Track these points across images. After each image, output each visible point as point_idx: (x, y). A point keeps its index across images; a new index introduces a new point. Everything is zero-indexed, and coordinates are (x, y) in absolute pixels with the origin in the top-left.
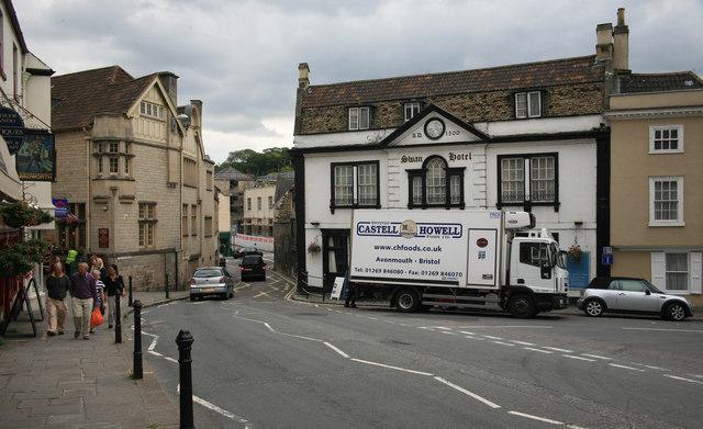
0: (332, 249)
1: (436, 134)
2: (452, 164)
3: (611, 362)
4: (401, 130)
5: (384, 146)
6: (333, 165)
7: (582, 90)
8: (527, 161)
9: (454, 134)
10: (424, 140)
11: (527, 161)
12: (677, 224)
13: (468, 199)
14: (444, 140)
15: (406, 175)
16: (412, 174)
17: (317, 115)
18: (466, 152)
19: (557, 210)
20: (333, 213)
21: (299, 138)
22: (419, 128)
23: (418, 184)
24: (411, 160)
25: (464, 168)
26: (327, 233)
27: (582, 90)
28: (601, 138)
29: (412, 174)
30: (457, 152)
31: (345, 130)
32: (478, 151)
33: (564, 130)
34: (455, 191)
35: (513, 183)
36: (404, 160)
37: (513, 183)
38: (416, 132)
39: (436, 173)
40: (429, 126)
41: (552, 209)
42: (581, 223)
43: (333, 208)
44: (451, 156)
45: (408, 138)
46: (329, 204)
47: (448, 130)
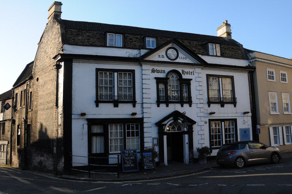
0: (97, 135)
1: (173, 57)
2: (185, 77)
3: (122, 184)
4: (152, 51)
5: (139, 61)
6: (97, 70)
7: (232, 48)
8: (116, 74)
9: (183, 58)
10: (166, 59)
11: (116, 74)
12: (277, 114)
13: (194, 99)
14: (178, 60)
15: (155, 81)
16: (159, 80)
17: (78, 35)
18: (191, 70)
19: (235, 106)
20: (97, 106)
21: (66, 47)
22: (162, 52)
23: (161, 86)
24: (158, 72)
25: (191, 79)
26: (91, 122)
27: (232, 48)
28: (251, 71)
29: (159, 80)
30: (187, 70)
31: (104, 45)
32: (198, 70)
33: (217, 63)
34: (185, 95)
35: (106, 88)
36: (153, 71)
37: (106, 88)
38: (161, 54)
39: (173, 81)
40: (168, 52)
41: (232, 105)
42: (214, 113)
43: (97, 103)
44: (183, 71)
45: (155, 57)
46: (207, 101)
47: (180, 55)
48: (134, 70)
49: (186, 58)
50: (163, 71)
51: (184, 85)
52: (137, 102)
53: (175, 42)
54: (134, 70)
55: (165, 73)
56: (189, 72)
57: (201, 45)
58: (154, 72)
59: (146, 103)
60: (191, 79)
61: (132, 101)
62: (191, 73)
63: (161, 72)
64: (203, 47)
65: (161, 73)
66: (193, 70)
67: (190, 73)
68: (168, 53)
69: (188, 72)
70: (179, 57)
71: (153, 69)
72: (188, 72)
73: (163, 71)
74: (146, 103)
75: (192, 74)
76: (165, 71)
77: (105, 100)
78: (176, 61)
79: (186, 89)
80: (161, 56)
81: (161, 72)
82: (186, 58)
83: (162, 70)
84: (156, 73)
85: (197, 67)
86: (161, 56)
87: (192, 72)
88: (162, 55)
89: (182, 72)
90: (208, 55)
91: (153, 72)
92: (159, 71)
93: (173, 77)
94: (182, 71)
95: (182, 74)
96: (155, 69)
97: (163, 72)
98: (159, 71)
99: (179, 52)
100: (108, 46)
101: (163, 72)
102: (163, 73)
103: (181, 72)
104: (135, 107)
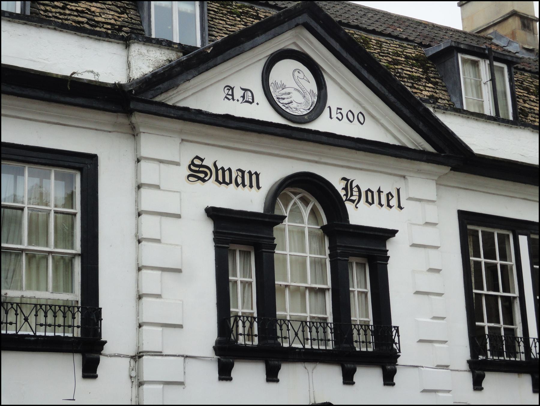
25: (393, 233)
48: (93, 158)
49: (361, 119)
50: (247, 176)
51: (352, 263)
52: (107, 350)
53: (313, 24)
54: (93, 158)
55: (259, 187)
56: (379, 191)
57: (416, 59)
58: (203, 180)
59: (159, 354)
60: (393, 233)
61: (326, 352)
62: (388, 201)
63: (240, 180)
64: (425, 72)
65: (237, 185)
66: (400, 184)
67: (384, 201)
68: (271, 81)
69: (375, 190)
70: (326, 111)
71: (197, 162)
72: (375, 190)
73: (247, 176)
74: (159, 354)
75: (394, 202)
76: (257, 175)
77: (315, 347)
78: (314, 126)
79: (246, 272)
80: (238, 93)
81: (240, 180)
82: (361, 119)
83: (243, 172)
84: (211, 183)
85: (419, 171)
86: (238, 93)
87: (395, 194)
88: (246, 90)
89: (345, 189)
90: (460, 111)
91: (199, 178)
92: (227, 174)
93: (296, 211)
94: (343, 184)
95: (344, 198)
96: (209, 162)
97: (247, 182)
98: (227, 174)
99: (331, 88)
100: (153, 36)
101: (247, 182)
102: (251, 186)
103: (339, 186)
104: (95, 377)
